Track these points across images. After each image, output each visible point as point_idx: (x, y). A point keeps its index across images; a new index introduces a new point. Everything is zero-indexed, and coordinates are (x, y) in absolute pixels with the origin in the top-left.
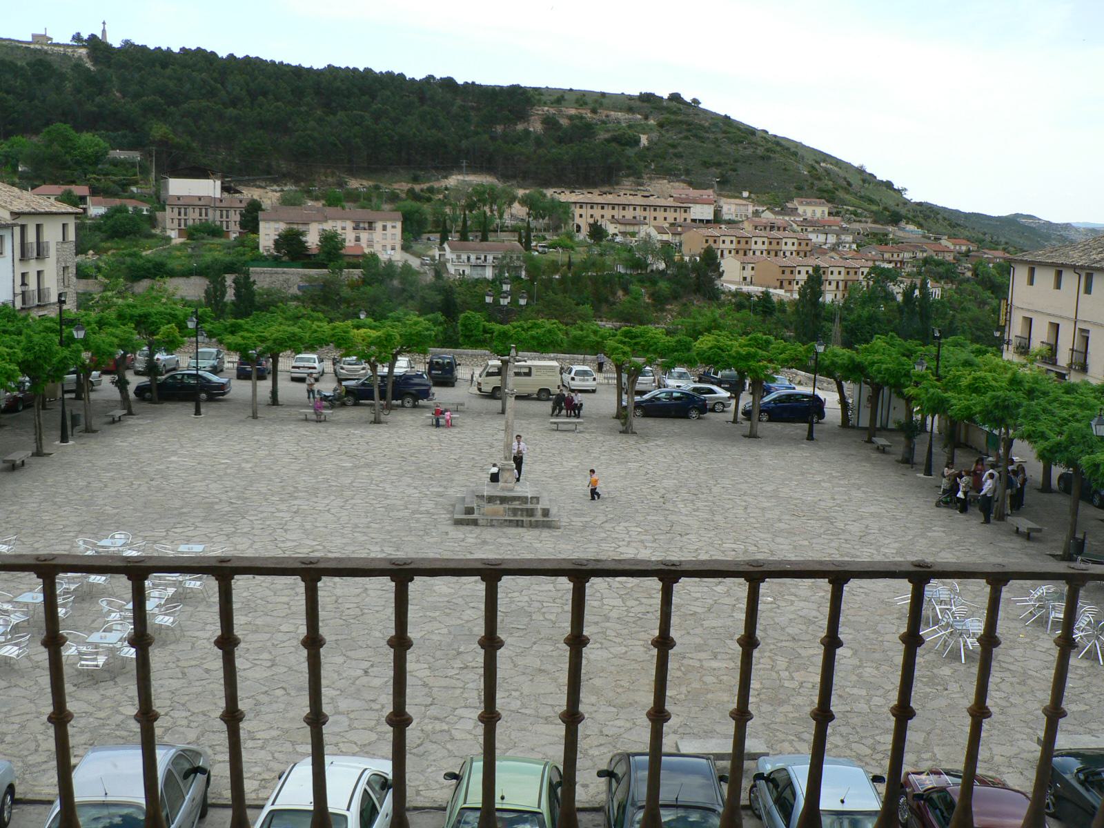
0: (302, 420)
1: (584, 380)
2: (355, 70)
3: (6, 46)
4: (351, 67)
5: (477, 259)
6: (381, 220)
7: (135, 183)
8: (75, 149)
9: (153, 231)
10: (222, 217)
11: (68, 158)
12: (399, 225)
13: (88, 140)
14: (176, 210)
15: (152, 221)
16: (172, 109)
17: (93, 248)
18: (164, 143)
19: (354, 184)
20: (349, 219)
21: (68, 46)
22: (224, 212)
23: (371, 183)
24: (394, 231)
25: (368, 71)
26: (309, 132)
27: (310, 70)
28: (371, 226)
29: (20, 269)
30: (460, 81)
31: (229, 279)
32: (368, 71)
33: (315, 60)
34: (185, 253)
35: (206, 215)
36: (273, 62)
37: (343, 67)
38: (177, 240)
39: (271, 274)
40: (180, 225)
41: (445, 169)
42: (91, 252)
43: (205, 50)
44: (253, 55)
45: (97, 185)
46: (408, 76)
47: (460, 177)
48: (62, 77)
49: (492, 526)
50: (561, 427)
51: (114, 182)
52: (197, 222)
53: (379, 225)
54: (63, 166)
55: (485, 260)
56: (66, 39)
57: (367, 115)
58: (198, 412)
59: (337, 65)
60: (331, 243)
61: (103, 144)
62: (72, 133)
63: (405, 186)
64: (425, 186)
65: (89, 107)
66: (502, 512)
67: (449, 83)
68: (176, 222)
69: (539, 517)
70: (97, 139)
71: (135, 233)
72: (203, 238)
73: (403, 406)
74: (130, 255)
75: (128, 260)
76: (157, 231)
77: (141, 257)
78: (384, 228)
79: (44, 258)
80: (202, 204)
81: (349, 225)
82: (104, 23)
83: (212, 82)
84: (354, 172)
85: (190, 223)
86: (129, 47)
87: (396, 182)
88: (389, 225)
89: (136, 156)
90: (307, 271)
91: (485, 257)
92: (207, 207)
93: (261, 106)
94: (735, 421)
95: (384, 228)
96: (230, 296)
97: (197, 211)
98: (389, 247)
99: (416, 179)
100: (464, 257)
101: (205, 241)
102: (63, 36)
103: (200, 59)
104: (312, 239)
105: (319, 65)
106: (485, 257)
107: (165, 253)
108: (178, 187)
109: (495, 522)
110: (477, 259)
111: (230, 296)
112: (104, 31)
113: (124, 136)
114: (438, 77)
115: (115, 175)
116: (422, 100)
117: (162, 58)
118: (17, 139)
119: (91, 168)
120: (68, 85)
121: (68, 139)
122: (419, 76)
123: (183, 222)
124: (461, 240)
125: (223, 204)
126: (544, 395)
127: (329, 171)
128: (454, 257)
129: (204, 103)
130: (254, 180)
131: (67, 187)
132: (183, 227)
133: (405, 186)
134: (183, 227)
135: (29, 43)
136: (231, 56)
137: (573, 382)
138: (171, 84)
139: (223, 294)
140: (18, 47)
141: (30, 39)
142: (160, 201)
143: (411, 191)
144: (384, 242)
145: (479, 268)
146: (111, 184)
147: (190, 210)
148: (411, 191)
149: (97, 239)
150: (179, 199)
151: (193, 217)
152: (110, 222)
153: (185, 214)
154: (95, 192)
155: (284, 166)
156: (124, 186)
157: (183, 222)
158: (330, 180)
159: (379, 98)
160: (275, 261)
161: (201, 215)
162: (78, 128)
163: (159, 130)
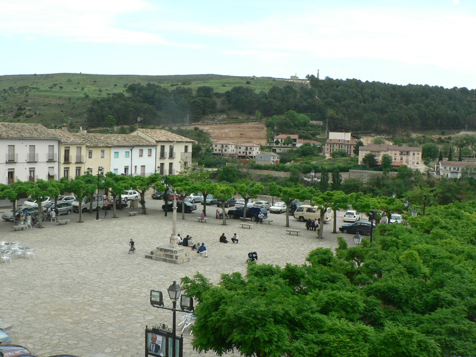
0: (197, 222)
1: (349, 217)
2: (421, 86)
3: (280, 81)
4: (419, 85)
5: (454, 169)
6: (412, 151)
7: (319, 134)
8: (296, 120)
9: (320, 154)
10: (348, 148)
11: (292, 124)
12: (420, 153)
13: (302, 117)
14: (329, 145)
15: (320, 150)
16: (338, 104)
17: (294, 160)
18: (332, 118)
19: (414, 136)
20: (398, 150)
21: (304, 80)
22: (349, 147)
23: (422, 135)
24: (418, 156)
25: (427, 86)
26: (395, 113)
27: (400, 87)
28: (408, 153)
29: (159, 162)
30: (470, 89)
31: (330, 175)
32: (442, 87)
33: (403, 82)
34: (328, 163)
35: (342, 147)
36: (385, 83)
37: (415, 84)
38: (328, 156)
39: (360, 173)
40: (330, 151)
41: (458, 129)
42: (293, 161)
43: (356, 80)
44: (376, 81)
45: (303, 134)
46: (445, 87)
47: (465, 132)
48: (295, 92)
49: (157, 260)
50: (291, 233)
51: (310, 133)
52: (338, 150)
53: (411, 153)
54: (290, 127)
55: (458, 170)
56: (304, 77)
57: (423, 105)
58: (166, 215)
59: (412, 84)
60: (387, 160)
61: (307, 118)
62: (296, 114)
63: (437, 136)
64: (447, 137)
65: (305, 104)
66: (162, 255)
67: (464, 90)
68: (329, 150)
69: (174, 259)
70: (305, 116)
71: (311, 154)
72: (338, 157)
73: (251, 220)
74: (306, 163)
75: (304, 164)
76: (321, 154)
77: (310, 164)
78: (414, 154)
79: (173, 158)
80: (340, 143)
81: (398, 153)
82: (318, 70)
83: (356, 93)
84: (415, 130)
85: (335, 150)
86: (328, 80)
87: (434, 134)
88: (416, 153)
89: (321, 123)
90: (376, 172)
91: (458, 168)
92: (342, 144)
93: (375, 102)
94: (335, 232)
95: (414, 154)
96: (330, 181)
97: (338, 146)
98: (416, 163)
99: (443, 134)
100: (448, 168)
101: (338, 158)
102: (302, 76)
103: (354, 84)
104: (379, 159)
105: (405, 83)
106: (458, 168)
107: (320, 163)
108: (334, 136)
109: (158, 259)
110: (454, 169)
111: (330, 181)
112: (318, 73)
113: (318, 115)
114: (459, 87)
115: (311, 131)
116: (450, 98)
117: (339, 83)
118: (275, 116)
119: (302, 128)
120: (298, 95)
121: (294, 116)
122: (450, 87)
123: (332, 150)
124: (448, 160)
125: (349, 143)
126: (302, 219)
127: (403, 129)
128: (443, 168)
129: (352, 101)
130: (370, 133)
131: (289, 135)
132: (332, 152)
133: (437, 136)
134: (332, 152)
135: (289, 79)
136: (367, 82)
137: (345, 218)
138: (339, 94)
139: (327, 180)
140: (284, 81)
141: (290, 78)
142: (324, 141)
143: (440, 139)
144: (413, 161)
145: (455, 174)
146: (308, 134)
147: (335, 145)
148: (440, 139)
149: (296, 156)
150: (339, 141)
151: (336, 148)
152: (302, 150)
153: (333, 147)
154: (300, 137)
155: (383, 127)
156: (314, 135)
157: (332, 150)
158: (403, 133)
159: (430, 98)
160: (363, 168)
161: (339, 147)
162: (299, 112)
163: (330, 112)
